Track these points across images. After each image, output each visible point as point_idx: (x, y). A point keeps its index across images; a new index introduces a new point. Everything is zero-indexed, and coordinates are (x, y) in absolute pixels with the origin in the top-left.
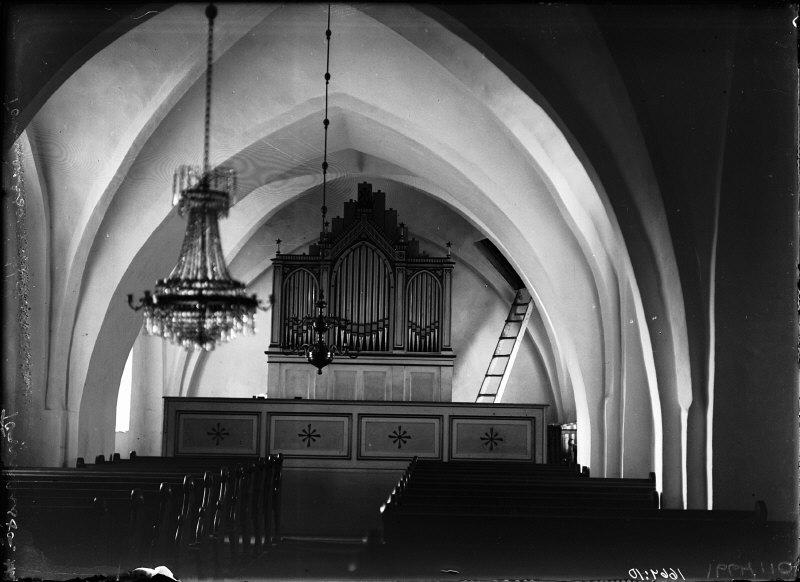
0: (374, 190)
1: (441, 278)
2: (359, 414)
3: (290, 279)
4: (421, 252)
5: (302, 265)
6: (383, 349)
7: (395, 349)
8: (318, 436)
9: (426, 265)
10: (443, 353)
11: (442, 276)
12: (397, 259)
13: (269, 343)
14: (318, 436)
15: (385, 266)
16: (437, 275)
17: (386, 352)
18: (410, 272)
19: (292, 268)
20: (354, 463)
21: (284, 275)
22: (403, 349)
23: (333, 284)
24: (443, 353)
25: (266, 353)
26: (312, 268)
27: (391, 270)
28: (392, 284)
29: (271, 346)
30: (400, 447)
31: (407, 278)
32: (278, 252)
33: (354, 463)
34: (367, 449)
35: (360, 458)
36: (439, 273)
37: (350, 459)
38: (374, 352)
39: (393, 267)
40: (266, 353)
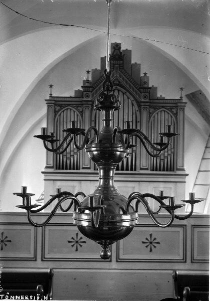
0: (123, 48)
1: (176, 114)
2: (192, 225)
3: (60, 115)
4: (159, 95)
5: (163, 107)
6: (132, 170)
7: (141, 169)
8: (158, 243)
9: (164, 105)
10: (178, 172)
11: (177, 113)
12: (143, 100)
13: (45, 165)
14: (158, 243)
15: (133, 105)
16: (172, 112)
17: (133, 172)
18: (152, 110)
19: (61, 106)
20: (39, 263)
21: (56, 112)
22: (147, 169)
23: (93, 119)
24: (178, 172)
25: (42, 172)
26: (77, 107)
27: (137, 109)
28: (138, 120)
29: (46, 167)
30: (77, 250)
31: (150, 114)
32: (51, 94)
33: (39, 263)
34: (198, 254)
35: (43, 259)
36: (174, 111)
37: (36, 260)
38: (129, 172)
39: (139, 106)
40: (42, 172)
